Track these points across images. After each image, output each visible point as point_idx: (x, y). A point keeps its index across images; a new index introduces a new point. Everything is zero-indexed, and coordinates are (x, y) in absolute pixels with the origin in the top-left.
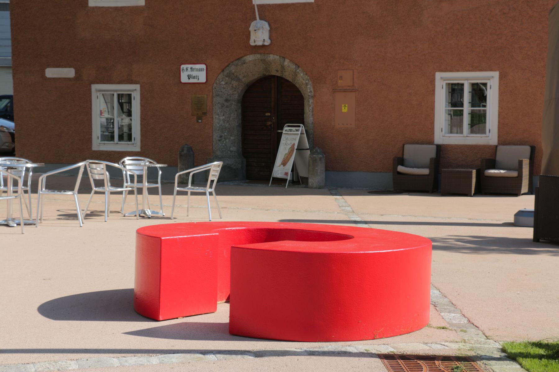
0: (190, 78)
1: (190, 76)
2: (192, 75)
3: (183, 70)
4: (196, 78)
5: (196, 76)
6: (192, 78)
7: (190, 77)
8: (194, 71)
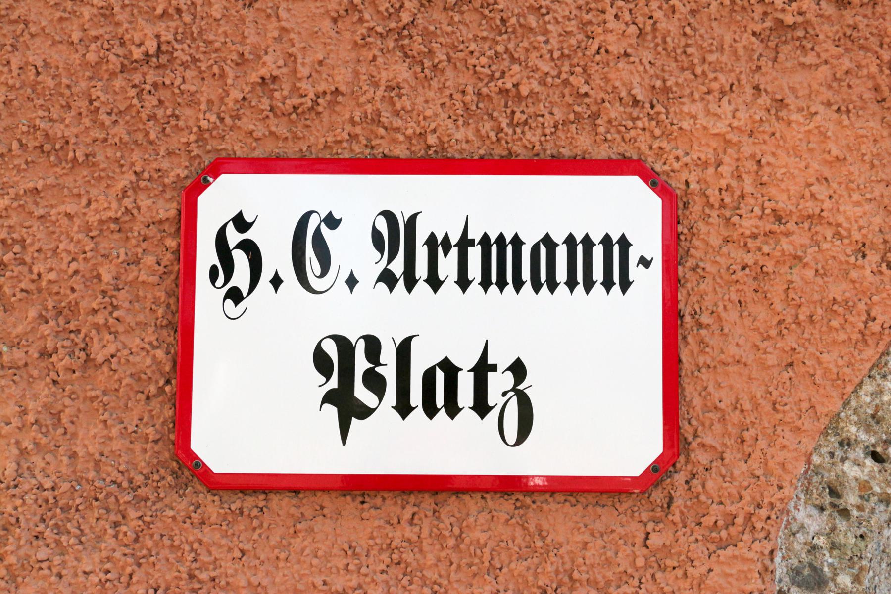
0: (362, 394)
1: (361, 364)
2: (404, 350)
3: (240, 259)
4: (481, 407)
5: (482, 369)
6: (404, 408)
7: (375, 383)
8: (435, 282)
